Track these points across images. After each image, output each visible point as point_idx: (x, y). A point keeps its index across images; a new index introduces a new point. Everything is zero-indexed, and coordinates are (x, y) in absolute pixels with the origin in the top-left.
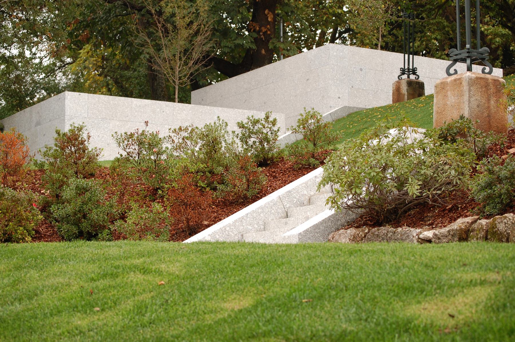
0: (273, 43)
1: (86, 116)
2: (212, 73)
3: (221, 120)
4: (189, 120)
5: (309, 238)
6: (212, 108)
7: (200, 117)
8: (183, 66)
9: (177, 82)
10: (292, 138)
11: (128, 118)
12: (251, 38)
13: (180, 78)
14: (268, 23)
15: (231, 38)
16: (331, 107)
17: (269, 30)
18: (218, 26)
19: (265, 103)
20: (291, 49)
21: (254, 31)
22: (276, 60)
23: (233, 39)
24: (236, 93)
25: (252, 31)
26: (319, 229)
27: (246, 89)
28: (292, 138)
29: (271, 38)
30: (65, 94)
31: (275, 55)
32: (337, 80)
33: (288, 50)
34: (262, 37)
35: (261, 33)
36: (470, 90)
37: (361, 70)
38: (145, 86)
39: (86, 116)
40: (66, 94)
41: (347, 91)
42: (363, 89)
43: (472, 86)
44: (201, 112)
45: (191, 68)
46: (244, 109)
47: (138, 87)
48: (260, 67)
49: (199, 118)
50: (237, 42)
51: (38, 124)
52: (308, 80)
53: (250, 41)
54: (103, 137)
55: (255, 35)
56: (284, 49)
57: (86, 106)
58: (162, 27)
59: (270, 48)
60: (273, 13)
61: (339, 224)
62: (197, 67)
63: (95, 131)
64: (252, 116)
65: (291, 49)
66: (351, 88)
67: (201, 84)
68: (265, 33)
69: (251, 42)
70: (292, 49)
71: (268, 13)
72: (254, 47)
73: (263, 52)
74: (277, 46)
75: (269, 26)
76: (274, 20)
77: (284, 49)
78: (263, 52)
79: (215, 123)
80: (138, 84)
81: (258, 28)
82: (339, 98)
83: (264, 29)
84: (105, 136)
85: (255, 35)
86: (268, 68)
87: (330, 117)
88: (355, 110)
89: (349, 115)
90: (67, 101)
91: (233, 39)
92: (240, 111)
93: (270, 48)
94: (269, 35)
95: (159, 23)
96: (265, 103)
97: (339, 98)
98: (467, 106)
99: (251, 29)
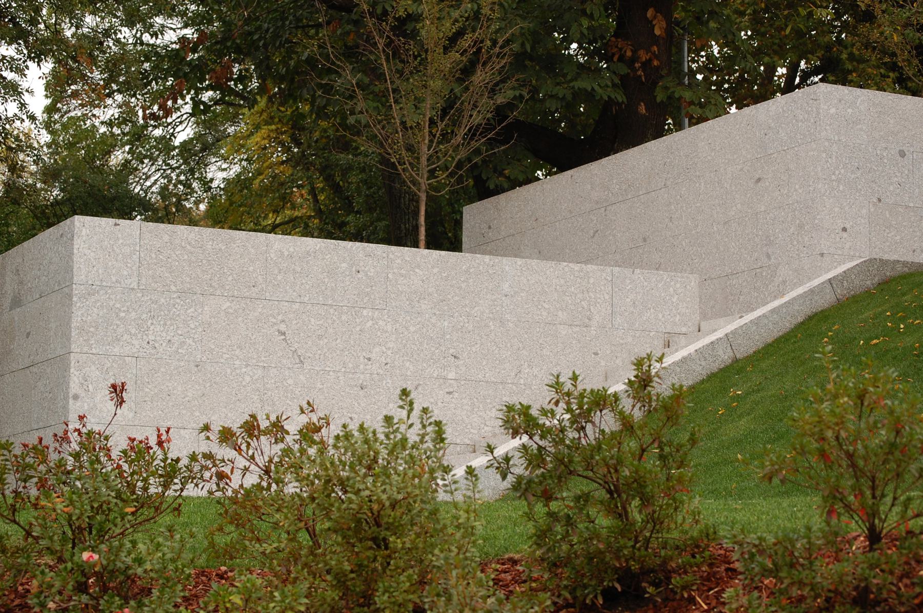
0: (667, 88)
1: (134, 285)
2: (519, 160)
3: (416, 412)
4: (430, 294)
6: (497, 259)
7: (463, 285)
8: (439, 143)
9: (424, 182)
10: (721, 353)
11: (256, 289)
12: (614, 77)
13: (432, 173)
14: (655, 40)
15: (564, 76)
16: (822, 255)
17: (657, 57)
18: (533, 48)
19: (645, 240)
20: (708, 102)
21: (621, 59)
22: (670, 131)
23: (569, 77)
24: (571, 212)
25: (615, 59)
27: (597, 203)
28: (721, 353)
29: (662, 77)
30: (73, 223)
31: (670, 121)
32: (839, 181)
33: (701, 106)
34: (640, 73)
35: (637, 65)
37: (902, 154)
38: (379, 188)
39: (134, 285)
40: (77, 223)
41: (864, 211)
42: (907, 207)
44: (467, 271)
45: (458, 149)
46: (586, 262)
47: (364, 190)
48: (627, 148)
49: (460, 288)
50: (578, 84)
51: (17, 302)
52: (759, 180)
53: (610, 84)
55: (624, 70)
56: (691, 103)
58: (388, 45)
59: (659, 100)
60: (668, 17)
62: (475, 144)
63: (158, 328)
64: (575, 378)
65: (708, 102)
66: (874, 205)
67: (492, 187)
68: (646, 65)
69: (614, 85)
70: (713, 101)
71: (655, 17)
72: (620, 97)
73: (642, 109)
74: (677, 95)
75: (655, 48)
76: (669, 31)
77: (691, 103)
78: (642, 109)
79: (388, 419)
80: (365, 182)
81: (629, 54)
82: (844, 230)
83: (644, 56)
84: (190, 341)
85: (624, 70)
86: (653, 146)
87: (828, 289)
88: (899, 268)
89: (885, 285)
90: (77, 243)
91: (569, 77)
92: (576, 267)
93: (659, 100)
94: (657, 68)
95: (381, 37)
96: (645, 240)
97: (844, 230)
99: (613, 55)
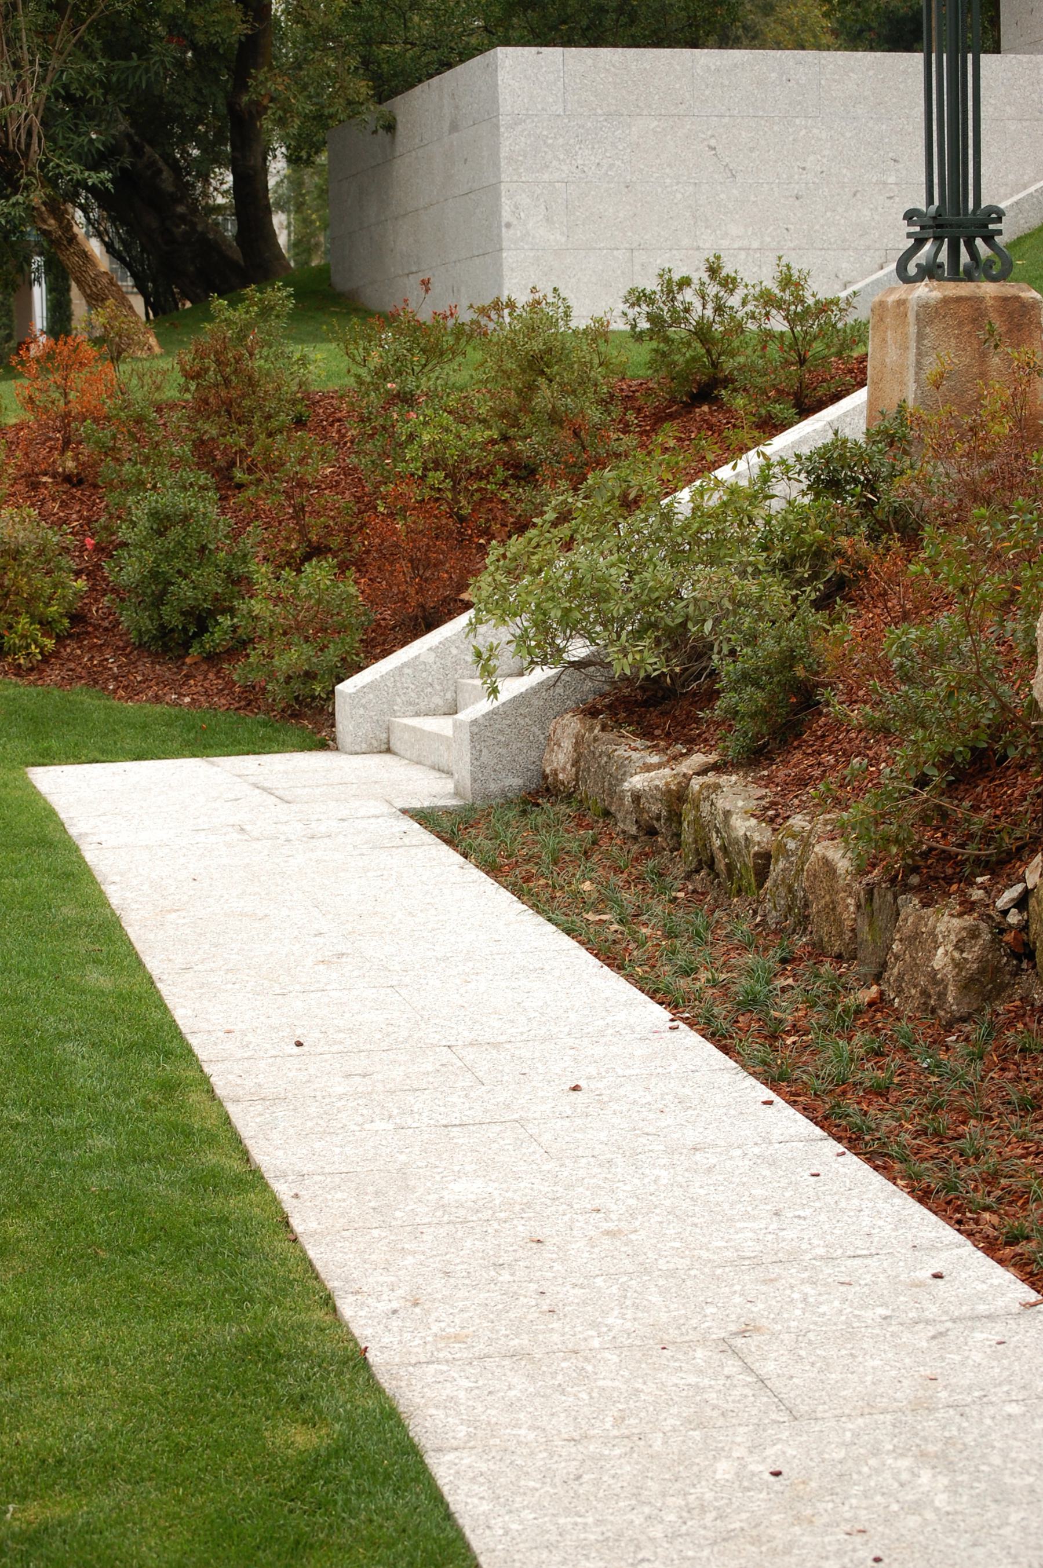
1: (561, 112)
4: (865, 98)
5: (501, 731)
7: (901, 86)
11: (683, 106)
26: (530, 705)
36: (920, 336)
39: (561, 112)
40: (500, 55)
43: (930, 322)
44: (905, 72)
51: (454, 127)
54: (611, 166)
57: (560, 84)
61: (586, 688)
84: (618, 163)
98: (912, 380)
